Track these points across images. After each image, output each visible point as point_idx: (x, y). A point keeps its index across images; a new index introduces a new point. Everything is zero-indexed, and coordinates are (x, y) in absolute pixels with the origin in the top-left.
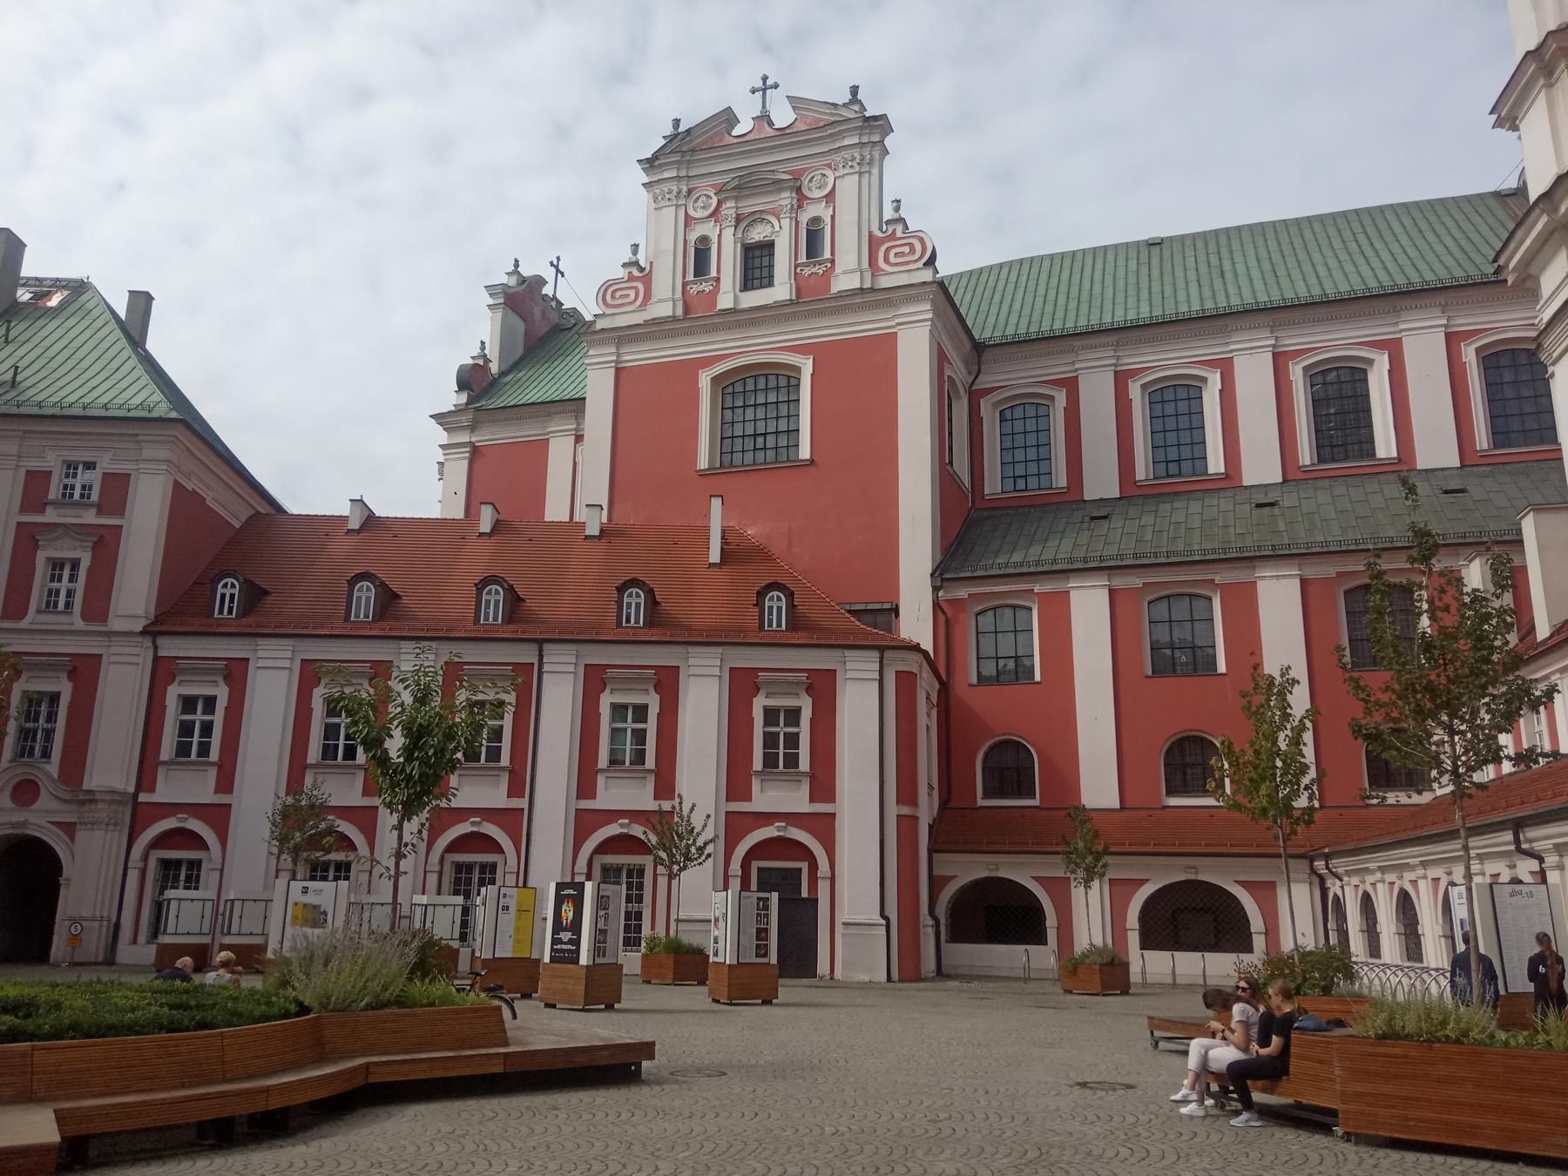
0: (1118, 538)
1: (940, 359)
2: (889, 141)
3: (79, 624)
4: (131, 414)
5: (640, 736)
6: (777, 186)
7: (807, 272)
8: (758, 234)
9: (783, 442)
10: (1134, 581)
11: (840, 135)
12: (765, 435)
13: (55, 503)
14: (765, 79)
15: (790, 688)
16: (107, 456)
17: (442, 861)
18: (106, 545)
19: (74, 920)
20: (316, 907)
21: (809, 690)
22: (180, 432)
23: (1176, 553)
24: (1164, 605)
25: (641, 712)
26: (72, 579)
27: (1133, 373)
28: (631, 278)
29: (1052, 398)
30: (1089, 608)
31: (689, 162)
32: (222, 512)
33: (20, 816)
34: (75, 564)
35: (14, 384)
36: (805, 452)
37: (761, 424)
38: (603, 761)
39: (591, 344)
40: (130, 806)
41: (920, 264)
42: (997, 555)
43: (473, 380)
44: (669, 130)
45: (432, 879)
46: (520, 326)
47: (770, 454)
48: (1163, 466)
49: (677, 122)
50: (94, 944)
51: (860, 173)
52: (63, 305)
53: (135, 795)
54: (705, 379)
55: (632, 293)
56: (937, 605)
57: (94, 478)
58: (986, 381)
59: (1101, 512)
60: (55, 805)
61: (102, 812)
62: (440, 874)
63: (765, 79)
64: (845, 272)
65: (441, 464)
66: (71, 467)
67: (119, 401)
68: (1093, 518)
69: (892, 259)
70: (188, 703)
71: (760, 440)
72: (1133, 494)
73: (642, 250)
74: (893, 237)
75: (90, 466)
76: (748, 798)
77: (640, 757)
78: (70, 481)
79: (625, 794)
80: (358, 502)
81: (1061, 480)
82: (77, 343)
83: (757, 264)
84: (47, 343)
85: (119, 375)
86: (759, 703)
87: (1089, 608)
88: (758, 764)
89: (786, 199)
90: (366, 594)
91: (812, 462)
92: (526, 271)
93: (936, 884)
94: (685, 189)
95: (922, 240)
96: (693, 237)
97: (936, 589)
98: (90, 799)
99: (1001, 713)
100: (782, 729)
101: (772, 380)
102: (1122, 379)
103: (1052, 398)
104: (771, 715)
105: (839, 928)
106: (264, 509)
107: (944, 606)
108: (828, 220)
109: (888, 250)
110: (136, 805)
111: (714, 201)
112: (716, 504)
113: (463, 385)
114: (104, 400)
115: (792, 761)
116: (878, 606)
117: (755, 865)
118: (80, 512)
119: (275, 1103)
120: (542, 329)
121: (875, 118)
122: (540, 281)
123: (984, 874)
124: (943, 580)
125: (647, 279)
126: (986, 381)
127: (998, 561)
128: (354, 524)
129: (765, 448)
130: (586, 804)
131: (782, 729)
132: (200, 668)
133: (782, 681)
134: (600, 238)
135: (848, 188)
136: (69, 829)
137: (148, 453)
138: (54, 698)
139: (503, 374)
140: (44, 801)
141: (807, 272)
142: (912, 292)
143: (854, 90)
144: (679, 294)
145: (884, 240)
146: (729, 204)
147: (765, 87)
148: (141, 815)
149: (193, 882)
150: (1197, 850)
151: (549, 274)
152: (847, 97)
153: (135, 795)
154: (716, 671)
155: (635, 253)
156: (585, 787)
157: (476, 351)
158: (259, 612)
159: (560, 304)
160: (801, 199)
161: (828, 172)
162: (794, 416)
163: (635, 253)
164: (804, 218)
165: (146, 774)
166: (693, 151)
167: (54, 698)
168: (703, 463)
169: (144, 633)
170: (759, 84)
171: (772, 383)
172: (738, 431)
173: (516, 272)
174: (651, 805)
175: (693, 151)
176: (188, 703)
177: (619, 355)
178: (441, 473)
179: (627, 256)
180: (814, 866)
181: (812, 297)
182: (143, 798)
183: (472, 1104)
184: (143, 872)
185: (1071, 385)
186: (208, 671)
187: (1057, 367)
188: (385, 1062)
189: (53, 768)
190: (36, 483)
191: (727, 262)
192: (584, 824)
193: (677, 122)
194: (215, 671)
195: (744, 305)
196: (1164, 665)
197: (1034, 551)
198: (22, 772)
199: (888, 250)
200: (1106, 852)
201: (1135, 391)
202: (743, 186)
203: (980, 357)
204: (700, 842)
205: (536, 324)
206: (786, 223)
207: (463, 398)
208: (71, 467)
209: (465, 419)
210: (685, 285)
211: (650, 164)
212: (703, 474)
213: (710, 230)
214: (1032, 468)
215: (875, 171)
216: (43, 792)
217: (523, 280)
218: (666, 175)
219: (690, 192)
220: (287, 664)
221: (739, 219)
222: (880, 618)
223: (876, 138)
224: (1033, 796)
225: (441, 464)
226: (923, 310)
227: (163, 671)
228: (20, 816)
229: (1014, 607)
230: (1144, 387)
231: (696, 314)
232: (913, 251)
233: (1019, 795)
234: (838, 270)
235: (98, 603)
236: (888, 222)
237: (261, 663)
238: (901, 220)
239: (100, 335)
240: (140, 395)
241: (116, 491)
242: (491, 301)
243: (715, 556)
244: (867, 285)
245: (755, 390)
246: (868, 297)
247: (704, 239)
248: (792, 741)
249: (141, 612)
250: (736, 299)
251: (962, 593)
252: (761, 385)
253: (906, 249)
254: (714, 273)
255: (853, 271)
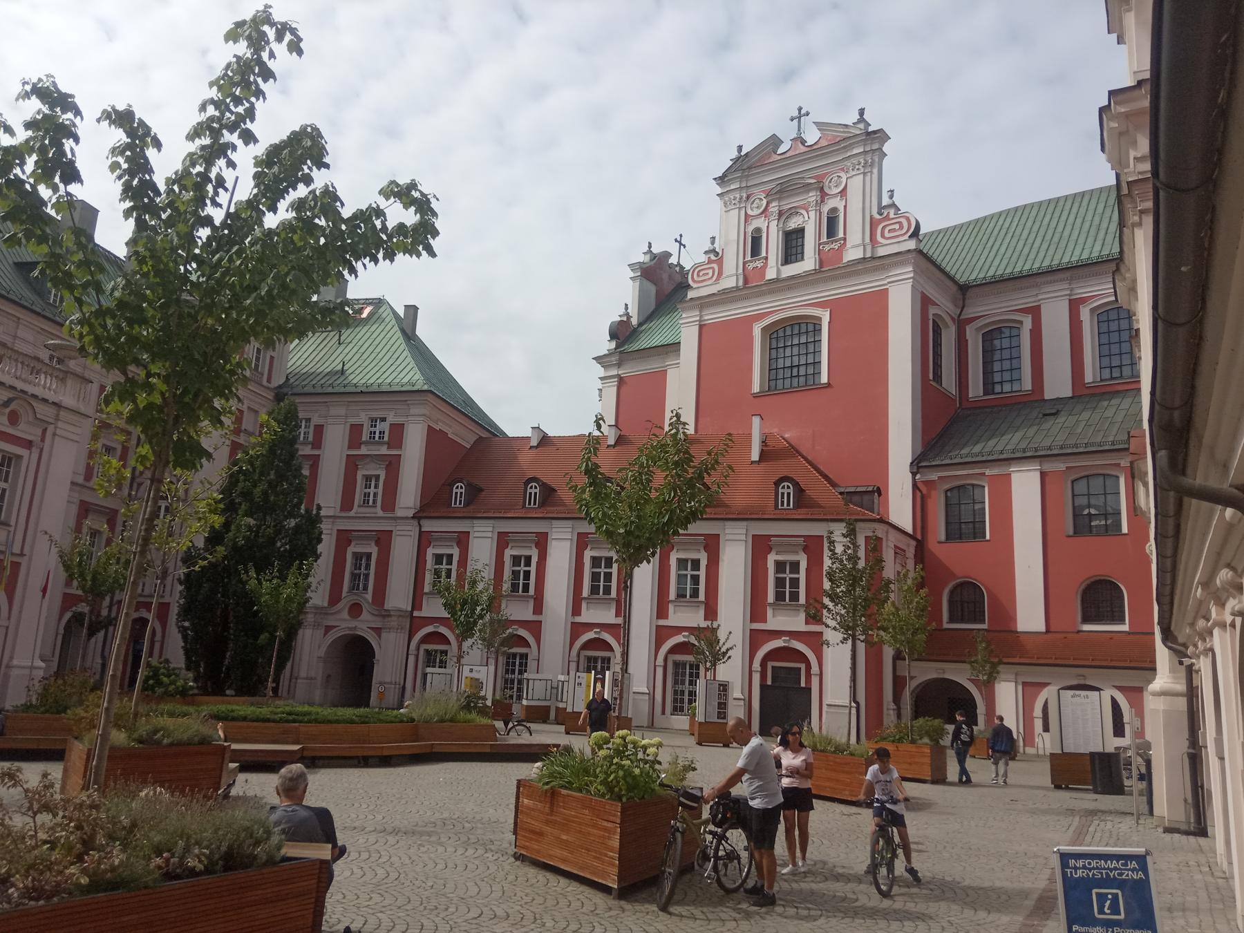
0: (1056, 433)
1: (923, 303)
2: (886, 148)
3: (380, 513)
4: (404, 389)
5: (695, 579)
6: (807, 188)
7: (827, 248)
8: (793, 224)
9: (811, 371)
10: (1060, 466)
11: (851, 146)
12: (798, 366)
13: (366, 443)
14: (800, 109)
15: (792, 549)
16: (392, 414)
17: (578, 655)
18: (393, 466)
19: (381, 684)
20: (477, 680)
21: (805, 549)
22: (430, 397)
23: (1093, 444)
24: (1084, 482)
25: (696, 564)
26: (376, 487)
27: (1083, 301)
28: (710, 261)
29: (1021, 322)
30: (1025, 487)
31: (748, 176)
32: (459, 441)
33: (353, 624)
34: (377, 477)
35: (343, 372)
36: (824, 379)
37: (796, 359)
38: (672, 595)
39: (684, 310)
40: (408, 620)
41: (906, 237)
42: (964, 446)
43: (622, 333)
44: (735, 154)
45: (573, 666)
46: (652, 289)
47: (802, 379)
48: (1108, 370)
49: (740, 148)
50: (392, 697)
51: (864, 174)
52: (371, 315)
53: (412, 612)
54: (757, 330)
55: (710, 272)
56: (915, 486)
57: (385, 426)
58: (970, 312)
59: (1056, 408)
60: (370, 617)
61: (394, 622)
62: (578, 662)
63: (800, 109)
64: (853, 247)
65: (600, 390)
66: (373, 421)
67: (397, 380)
68: (1045, 415)
69: (887, 235)
70: (438, 559)
71: (795, 370)
72: (1084, 395)
73: (717, 240)
74: (887, 218)
75: (383, 420)
76: (765, 621)
77: (695, 593)
78: (373, 429)
79: (686, 617)
80: (536, 429)
81: (1027, 385)
82: (376, 342)
83: (792, 245)
84: (360, 343)
85: (398, 363)
86: (772, 559)
87: (1025, 487)
88: (771, 598)
89: (813, 197)
90: (534, 489)
91: (829, 385)
92: (655, 250)
93: (899, 683)
94: (745, 195)
95: (908, 219)
96: (750, 229)
97: (914, 474)
98: (387, 615)
99: (959, 559)
100: (788, 576)
101: (803, 326)
102: (1075, 305)
103: (1021, 322)
104: (780, 566)
105: (825, 708)
106: (485, 435)
107: (920, 486)
108: (842, 209)
109: (884, 228)
110: (412, 617)
111: (765, 202)
112: (756, 421)
113: (613, 335)
114: (388, 381)
115: (794, 596)
116: (863, 489)
117: (770, 664)
118: (377, 447)
119: (386, 753)
120: (669, 288)
121: (875, 132)
122: (668, 255)
123: (935, 676)
124: (919, 468)
125: (720, 262)
126: (970, 312)
127: (963, 452)
128: (534, 443)
129: (798, 376)
130: (662, 622)
131: (788, 576)
132: (444, 537)
133: (787, 543)
134: (699, 226)
135: (856, 185)
136: (378, 631)
137: (413, 411)
138: (369, 556)
139: (640, 325)
140: (365, 615)
141: (827, 248)
142: (899, 258)
143: (862, 112)
144: (741, 271)
145: (880, 221)
146: (774, 204)
147: (801, 115)
148: (415, 624)
149: (443, 665)
150: (1143, 665)
151: (673, 248)
152: (856, 117)
153: (412, 612)
154: (743, 537)
155: (713, 243)
156: (661, 612)
157: (622, 311)
158: (477, 503)
159: (682, 268)
160: (823, 195)
161: (842, 174)
162: (817, 352)
163: (713, 243)
164: (826, 209)
165: (417, 603)
166: (750, 168)
167: (369, 556)
168: (756, 388)
169: (413, 517)
170: (796, 114)
171: (803, 329)
172: (781, 364)
173: (650, 251)
174: (704, 624)
175: (750, 168)
176: (438, 559)
177: (701, 316)
178: (600, 396)
179: (708, 246)
180: (809, 667)
181: (829, 268)
182: (416, 614)
183: (469, 764)
184: (417, 656)
185: (1035, 312)
186: (446, 539)
187: (1025, 299)
188: (440, 745)
189: (369, 596)
190: (356, 429)
191: (773, 245)
192: (661, 634)
193: (740, 148)
194: (451, 539)
195: (784, 275)
196: (1082, 525)
197: (977, 449)
198: (353, 599)
199: (884, 228)
200: (1001, 663)
201: (1085, 314)
202: (782, 191)
203: (964, 295)
204: (724, 649)
205: (663, 284)
206: (812, 214)
207: (613, 345)
208: (373, 421)
209: (614, 359)
210: (744, 263)
211: (722, 180)
212: (756, 396)
213: (761, 223)
214: (1007, 376)
215: (875, 171)
216: (364, 611)
217: (654, 257)
218: (733, 187)
219: (748, 198)
220: (490, 535)
221: (780, 214)
222: (866, 498)
223: (876, 146)
224: (983, 621)
225: (600, 390)
226: (907, 271)
227: (424, 540)
228: (353, 624)
229: (973, 485)
230: (1093, 310)
231: (751, 285)
232: (901, 227)
233: (975, 621)
234: (848, 246)
235: (390, 502)
236: (885, 207)
237: (477, 534)
238: (893, 205)
239: (389, 335)
240: (409, 375)
241: (398, 432)
242: (632, 274)
243: (755, 456)
244: (869, 255)
245: (791, 334)
246: (873, 263)
247: (758, 230)
248: (795, 583)
249: (411, 505)
250: (778, 271)
251: (934, 476)
252: (796, 331)
253: (897, 226)
254: (764, 254)
255: (858, 246)
